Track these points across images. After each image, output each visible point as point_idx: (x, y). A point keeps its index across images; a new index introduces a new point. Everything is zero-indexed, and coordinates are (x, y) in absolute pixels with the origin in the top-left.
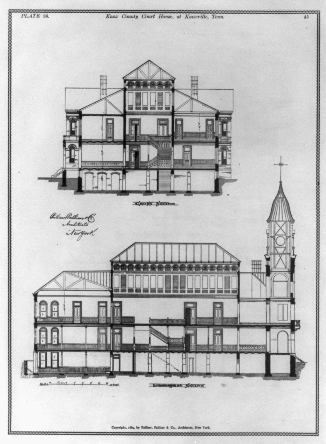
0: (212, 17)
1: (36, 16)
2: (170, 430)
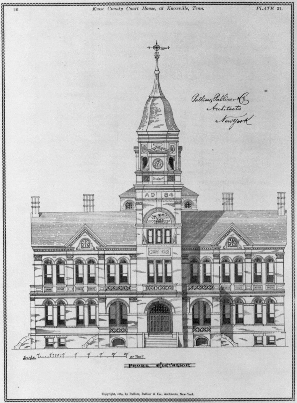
0: (193, 8)
1: (270, 9)
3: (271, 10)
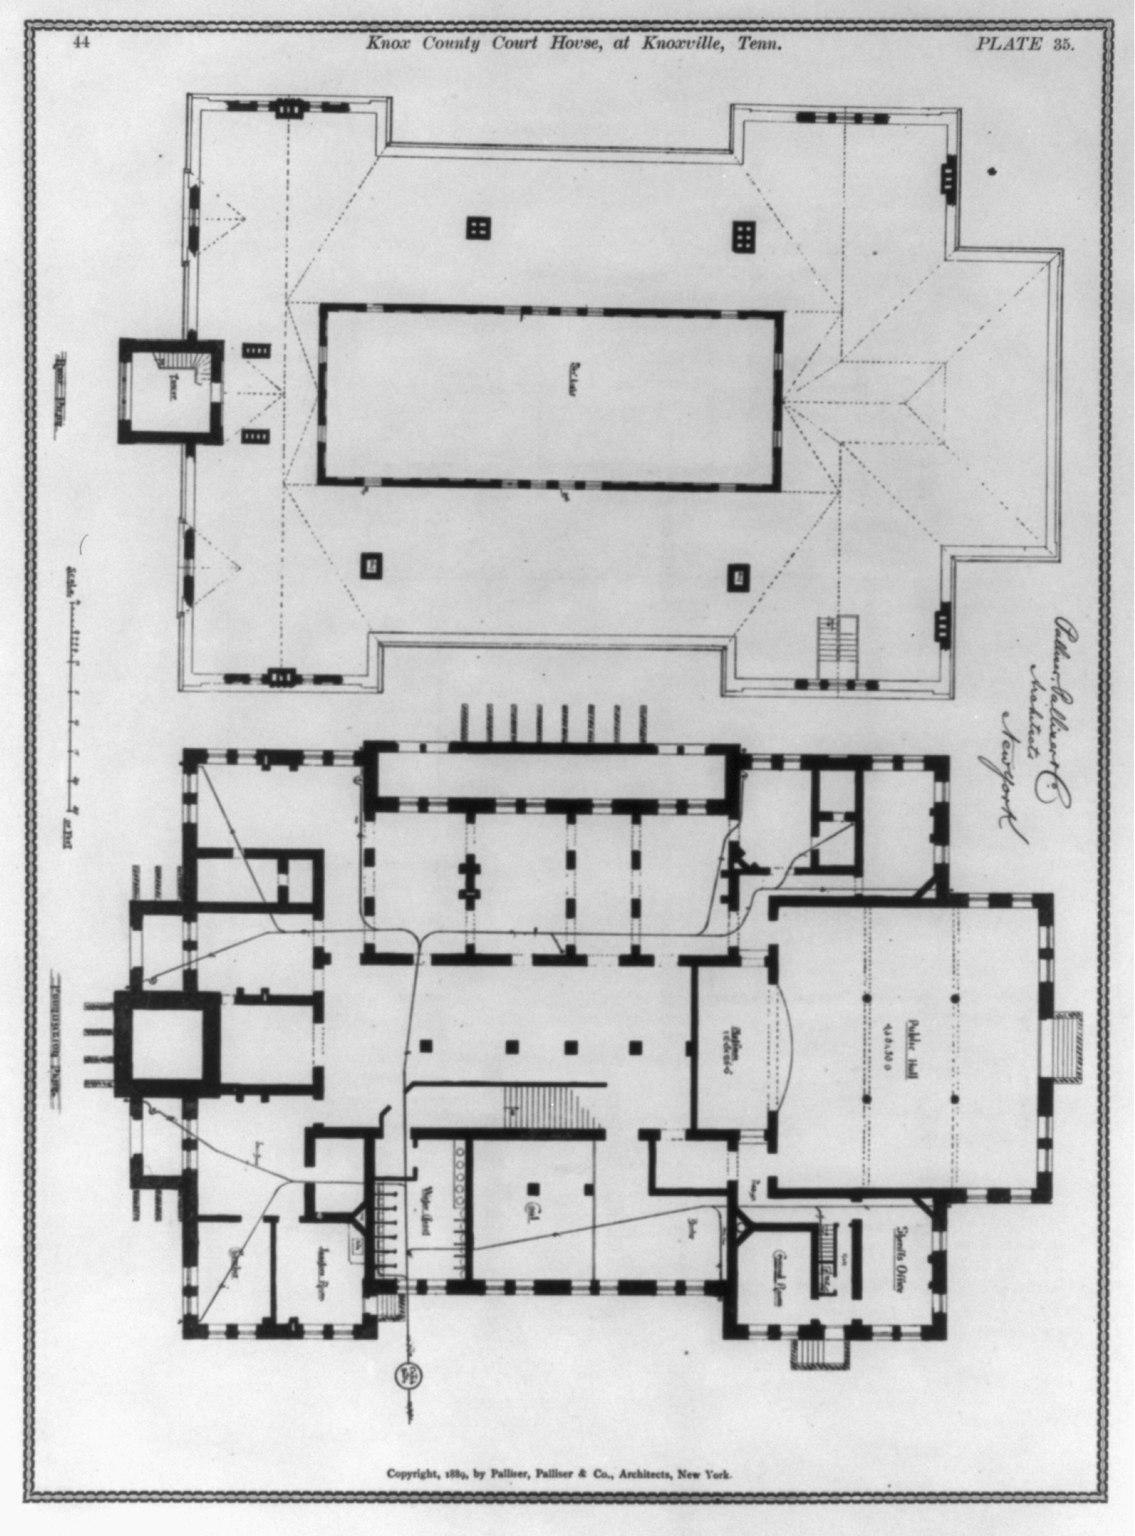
1: (1027, 44)
2: (591, 1485)
3: (1032, 48)
